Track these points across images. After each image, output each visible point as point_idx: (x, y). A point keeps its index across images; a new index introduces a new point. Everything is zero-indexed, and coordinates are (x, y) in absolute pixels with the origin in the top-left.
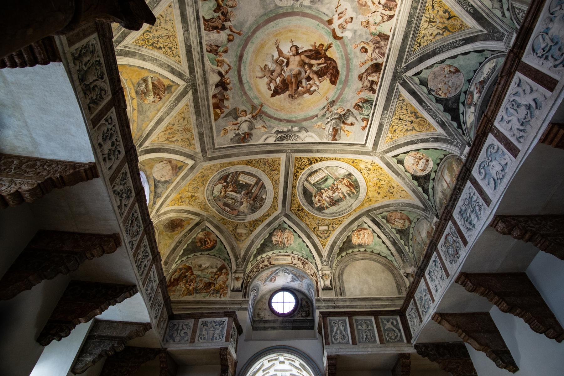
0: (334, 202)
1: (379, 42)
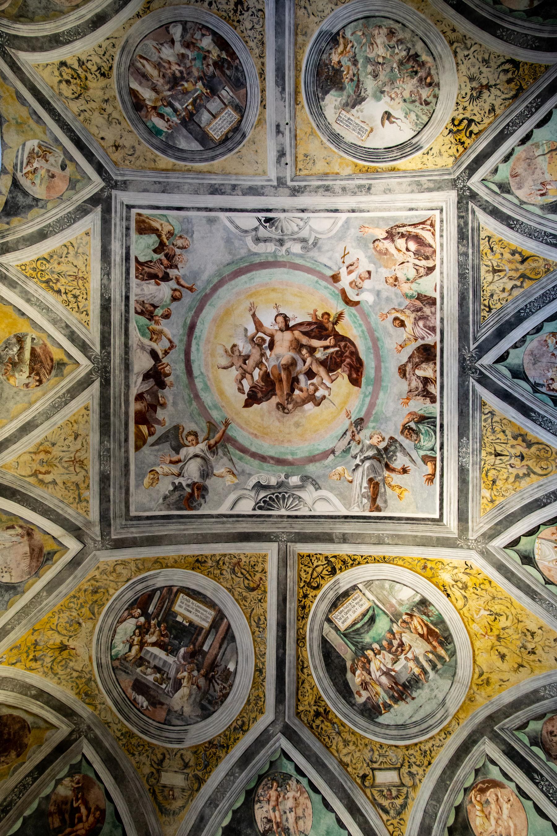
0: (403, 690)
1: (420, 310)
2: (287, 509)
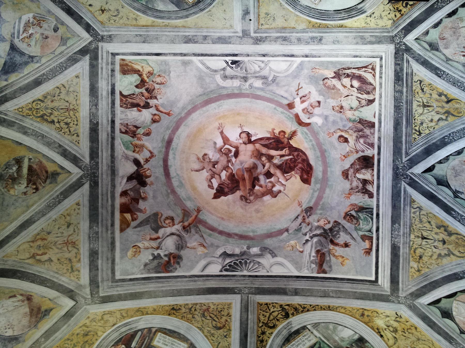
2: (248, 270)
